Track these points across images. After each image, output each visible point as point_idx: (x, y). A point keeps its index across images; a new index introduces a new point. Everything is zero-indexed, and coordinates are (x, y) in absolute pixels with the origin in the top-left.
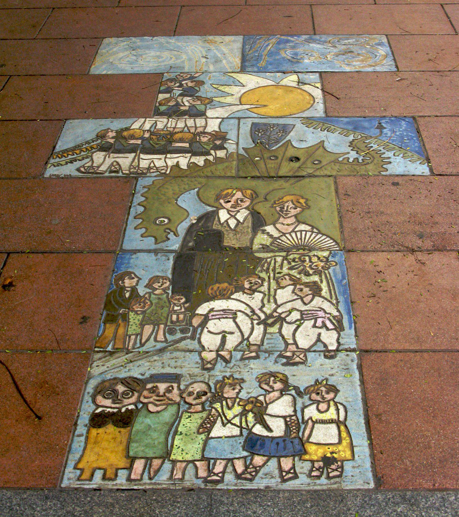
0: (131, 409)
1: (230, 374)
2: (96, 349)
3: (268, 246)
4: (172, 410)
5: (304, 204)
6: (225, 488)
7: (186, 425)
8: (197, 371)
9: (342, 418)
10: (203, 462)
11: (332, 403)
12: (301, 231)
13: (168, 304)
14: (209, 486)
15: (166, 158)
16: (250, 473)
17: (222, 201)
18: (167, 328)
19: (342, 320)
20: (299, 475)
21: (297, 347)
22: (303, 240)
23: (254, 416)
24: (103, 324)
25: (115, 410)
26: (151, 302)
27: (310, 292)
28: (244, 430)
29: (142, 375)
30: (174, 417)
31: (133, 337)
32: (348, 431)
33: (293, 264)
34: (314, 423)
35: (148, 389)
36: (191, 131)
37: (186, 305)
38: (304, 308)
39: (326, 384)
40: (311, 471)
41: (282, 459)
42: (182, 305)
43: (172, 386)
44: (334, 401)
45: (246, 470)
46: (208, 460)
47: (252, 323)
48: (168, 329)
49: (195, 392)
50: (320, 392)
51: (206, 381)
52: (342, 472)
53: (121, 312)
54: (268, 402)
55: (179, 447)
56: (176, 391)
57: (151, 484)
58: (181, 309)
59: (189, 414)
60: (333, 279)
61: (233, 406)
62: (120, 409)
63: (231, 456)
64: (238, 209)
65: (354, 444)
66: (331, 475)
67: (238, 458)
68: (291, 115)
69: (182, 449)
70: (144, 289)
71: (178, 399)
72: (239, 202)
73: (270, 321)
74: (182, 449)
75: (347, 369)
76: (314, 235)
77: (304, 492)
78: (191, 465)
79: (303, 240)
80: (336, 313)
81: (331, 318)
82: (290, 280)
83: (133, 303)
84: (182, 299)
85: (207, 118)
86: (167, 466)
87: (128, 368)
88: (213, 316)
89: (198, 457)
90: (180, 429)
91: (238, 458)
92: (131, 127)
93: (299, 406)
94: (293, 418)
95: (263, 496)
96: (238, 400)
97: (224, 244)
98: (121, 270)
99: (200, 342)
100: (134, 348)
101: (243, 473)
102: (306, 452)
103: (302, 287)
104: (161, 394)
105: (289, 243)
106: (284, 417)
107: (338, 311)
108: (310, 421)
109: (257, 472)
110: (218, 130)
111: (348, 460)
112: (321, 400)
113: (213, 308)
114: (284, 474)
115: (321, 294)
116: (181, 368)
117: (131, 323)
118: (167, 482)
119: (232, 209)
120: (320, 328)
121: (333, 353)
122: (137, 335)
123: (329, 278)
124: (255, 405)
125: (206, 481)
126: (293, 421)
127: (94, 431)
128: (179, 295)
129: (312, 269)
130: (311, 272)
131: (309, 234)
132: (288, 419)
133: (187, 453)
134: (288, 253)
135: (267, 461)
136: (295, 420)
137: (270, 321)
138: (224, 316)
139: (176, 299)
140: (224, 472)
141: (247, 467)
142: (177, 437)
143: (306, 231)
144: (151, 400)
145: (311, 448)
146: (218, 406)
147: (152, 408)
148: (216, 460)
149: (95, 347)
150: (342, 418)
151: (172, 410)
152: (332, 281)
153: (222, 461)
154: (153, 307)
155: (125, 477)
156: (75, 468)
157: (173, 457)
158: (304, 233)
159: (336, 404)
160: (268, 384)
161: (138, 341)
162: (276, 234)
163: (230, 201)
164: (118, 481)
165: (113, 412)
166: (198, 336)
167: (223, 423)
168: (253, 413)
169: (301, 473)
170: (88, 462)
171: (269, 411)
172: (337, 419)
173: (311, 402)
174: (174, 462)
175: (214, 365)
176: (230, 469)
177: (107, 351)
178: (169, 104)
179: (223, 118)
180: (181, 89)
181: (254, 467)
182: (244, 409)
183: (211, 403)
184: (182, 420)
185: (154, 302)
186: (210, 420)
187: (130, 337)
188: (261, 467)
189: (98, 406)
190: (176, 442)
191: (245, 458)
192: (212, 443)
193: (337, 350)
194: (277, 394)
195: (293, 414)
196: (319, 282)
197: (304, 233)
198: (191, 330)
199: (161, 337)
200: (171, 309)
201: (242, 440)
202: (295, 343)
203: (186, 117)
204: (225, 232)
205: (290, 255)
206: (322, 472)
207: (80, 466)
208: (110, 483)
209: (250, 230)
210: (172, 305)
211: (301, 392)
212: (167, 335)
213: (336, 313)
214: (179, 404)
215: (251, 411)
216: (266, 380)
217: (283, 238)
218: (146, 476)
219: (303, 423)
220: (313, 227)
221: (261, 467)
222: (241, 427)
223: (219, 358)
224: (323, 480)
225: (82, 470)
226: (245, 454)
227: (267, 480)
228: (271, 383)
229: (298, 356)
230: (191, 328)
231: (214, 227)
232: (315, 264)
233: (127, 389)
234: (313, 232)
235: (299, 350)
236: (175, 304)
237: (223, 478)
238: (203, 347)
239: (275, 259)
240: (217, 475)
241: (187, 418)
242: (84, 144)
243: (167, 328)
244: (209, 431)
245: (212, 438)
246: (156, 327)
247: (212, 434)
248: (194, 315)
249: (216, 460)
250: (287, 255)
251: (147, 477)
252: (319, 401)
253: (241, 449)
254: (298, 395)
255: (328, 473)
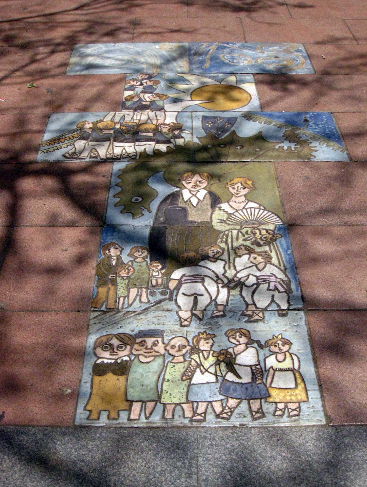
0: (126, 360)
1: (204, 330)
2: (92, 309)
3: (225, 221)
4: (160, 360)
5: (251, 185)
6: (208, 426)
7: (171, 374)
8: (177, 327)
9: (296, 367)
10: (188, 404)
11: (287, 354)
12: (251, 208)
13: (148, 271)
14: (195, 424)
15: (135, 145)
16: (226, 413)
17: (184, 183)
18: (149, 291)
19: (290, 284)
20: (266, 414)
21: (256, 307)
22: (253, 216)
23: (226, 365)
24: (96, 288)
25: (113, 361)
26: (134, 269)
27: (262, 260)
28: (219, 378)
29: (133, 331)
30: (162, 367)
31: (122, 299)
32: (302, 377)
33: (247, 236)
34: (275, 370)
35: (138, 343)
36: (154, 123)
37: (163, 271)
38: (258, 274)
39: (282, 338)
40: (276, 411)
41: (251, 401)
42: (159, 271)
43: (157, 341)
44: (289, 352)
45: (223, 411)
46: (192, 402)
47: (218, 287)
48: (150, 291)
49: (177, 346)
50: (277, 345)
51: (185, 336)
52: (300, 411)
53: (110, 277)
54: (236, 353)
55: (167, 392)
56: (161, 345)
57: (147, 423)
58: (159, 275)
59: (174, 364)
60: (281, 250)
61: (208, 357)
62: (116, 360)
63: (211, 400)
64: (198, 188)
65: (308, 389)
66: (292, 414)
67: (216, 401)
68: (233, 109)
69: (170, 394)
70: (128, 257)
71: (163, 351)
72: (198, 183)
73: (232, 285)
74: (170, 394)
75: (298, 325)
76: (262, 211)
77: (271, 429)
78: (178, 407)
79: (253, 216)
80: (286, 279)
81: (282, 282)
82: (246, 249)
83: (119, 269)
84: (158, 266)
85: (166, 111)
86: (160, 407)
87: (120, 326)
88: (185, 280)
89: (183, 400)
90: (167, 377)
91: (216, 401)
92: (103, 119)
93: (261, 357)
94: (258, 367)
95: (239, 432)
96: (212, 352)
97: (190, 219)
98: (107, 242)
99: (176, 303)
100: (123, 308)
101: (222, 413)
102: (270, 396)
103: (256, 256)
104: (149, 347)
105: (242, 218)
106: (251, 366)
107: (287, 276)
108: (271, 370)
109: (232, 412)
110: (175, 122)
111: (304, 402)
112: (279, 352)
113: (185, 274)
114: (254, 413)
115: (271, 262)
116: (163, 324)
117: (119, 287)
118: (161, 422)
119: (193, 189)
120: (274, 290)
121: (284, 312)
122: (125, 297)
123: (277, 248)
124: (226, 356)
125: (191, 420)
126: (257, 369)
127: (97, 379)
128: (156, 263)
129: (262, 240)
130: (262, 243)
131: (257, 210)
132: (253, 368)
133: (174, 397)
134: (241, 226)
135: (239, 403)
136: (259, 369)
137: (232, 285)
138: (194, 281)
139: (154, 266)
140: (205, 413)
141: (224, 408)
142: (165, 384)
143: (255, 208)
144: (141, 352)
145: (274, 392)
146: (195, 357)
147: (142, 359)
148: (198, 402)
149: (92, 307)
150: (296, 367)
151: (160, 360)
152: (279, 251)
153: (203, 403)
154: (136, 273)
155: (126, 417)
156: (85, 409)
157: (163, 400)
158: (253, 210)
159: (291, 354)
160: (235, 338)
161: (126, 302)
162: (230, 211)
163: (190, 183)
164: (120, 421)
165: (111, 363)
166: (174, 298)
167: (201, 372)
168: (225, 363)
169: (267, 413)
170: (94, 404)
171: (237, 361)
172: (292, 368)
173: (271, 353)
174: (165, 405)
175: (190, 322)
176: (210, 410)
177: (101, 311)
178: (133, 100)
179: (179, 112)
180: (142, 87)
181: (229, 408)
182: (218, 360)
183: (191, 355)
184: (168, 369)
185: (137, 269)
186: (191, 369)
187: (119, 299)
188: (235, 408)
189: (99, 358)
190: (165, 388)
191: (221, 400)
192: (195, 389)
193: (288, 309)
194: (243, 347)
195: (257, 363)
196: (269, 252)
197: (253, 210)
198: (168, 292)
199: (144, 299)
200: (151, 275)
201: (218, 385)
202: (254, 304)
203: (148, 111)
204: (189, 209)
205: (244, 228)
206: (284, 412)
207: (89, 408)
208: (115, 422)
209: (209, 207)
210: (151, 272)
211: (262, 345)
212: (149, 296)
213: (286, 279)
214: (164, 355)
215: (223, 361)
216: (233, 335)
217: (236, 214)
218: (143, 416)
219: (266, 370)
220: (260, 205)
221: (235, 408)
222: (217, 376)
223: (193, 317)
224: (285, 418)
225: (90, 411)
226: (222, 397)
227: (241, 419)
228: (238, 338)
229: (257, 315)
230: (168, 291)
231: (180, 205)
232: (264, 236)
233: (121, 343)
234: (260, 209)
235: (258, 309)
236: (153, 270)
237: (205, 417)
238: (179, 307)
239: (231, 232)
240: (200, 415)
241: (172, 368)
242: (67, 134)
243: (149, 291)
244: (191, 379)
245: (194, 384)
246: (140, 290)
247: (193, 381)
248: (169, 280)
249: (198, 402)
250: (242, 228)
251: (144, 418)
252: (277, 352)
253: (218, 393)
254: (260, 347)
255: (289, 413)
